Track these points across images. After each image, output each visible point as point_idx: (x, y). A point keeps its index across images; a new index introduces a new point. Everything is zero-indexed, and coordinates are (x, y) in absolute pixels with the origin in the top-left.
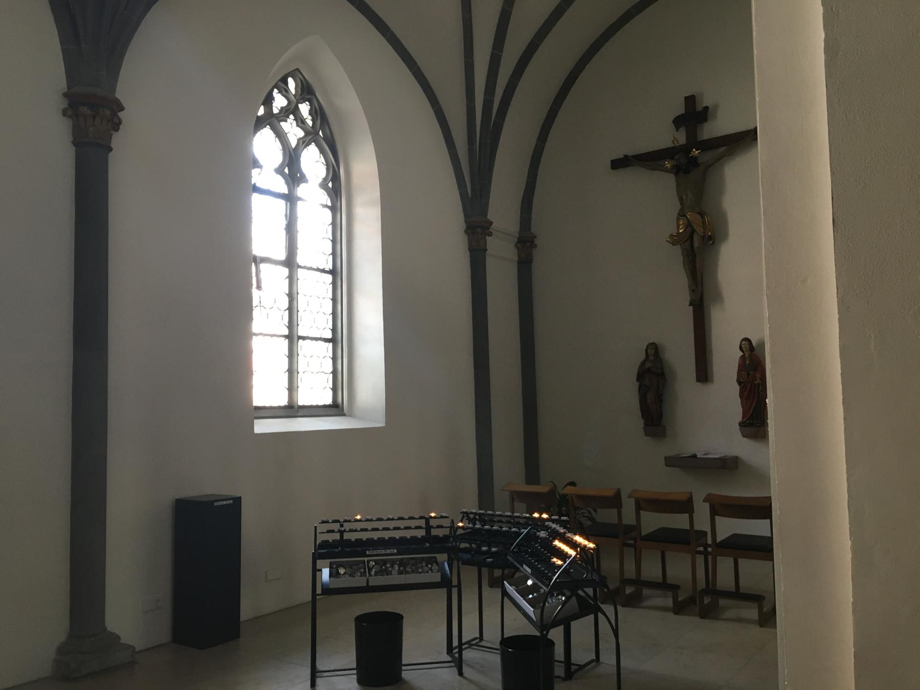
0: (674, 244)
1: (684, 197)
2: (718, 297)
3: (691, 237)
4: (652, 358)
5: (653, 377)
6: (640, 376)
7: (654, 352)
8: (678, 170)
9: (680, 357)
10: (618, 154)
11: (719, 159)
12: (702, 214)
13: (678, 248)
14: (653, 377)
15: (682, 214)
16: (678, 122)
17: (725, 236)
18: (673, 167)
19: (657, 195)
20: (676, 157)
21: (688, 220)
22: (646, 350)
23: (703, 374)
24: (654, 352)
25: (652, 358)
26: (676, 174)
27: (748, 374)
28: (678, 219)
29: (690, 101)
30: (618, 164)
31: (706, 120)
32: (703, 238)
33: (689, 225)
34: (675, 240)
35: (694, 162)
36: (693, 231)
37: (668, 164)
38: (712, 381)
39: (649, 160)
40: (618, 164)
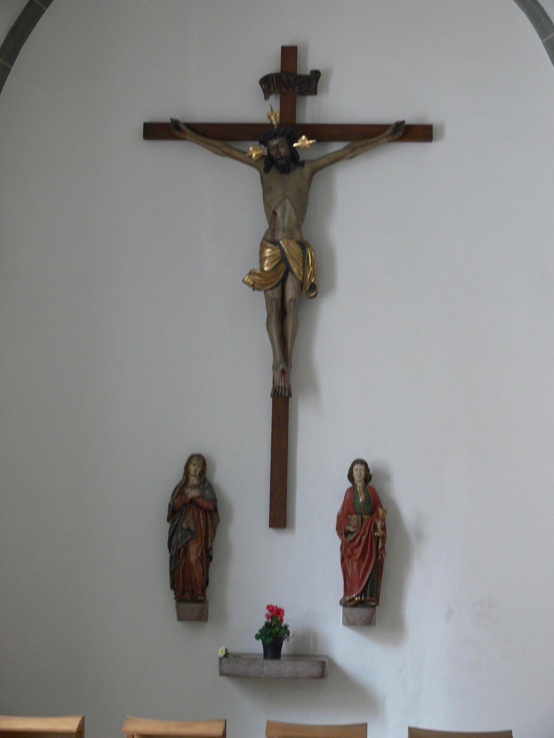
0: (254, 287)
1: (279, 212)
2: (312, 385)
3: (283, 282)
4: (193, 481)
5: (194, 518)
6: (175, 512)
7: (198, 468)
8: (269, 165)
9: (243, 486)
10: (163, 115)
11: (336, 159)
12: (303, 245)
13: (260, 296)
14: (194, 518)
15: (270, 239)
16: (269, 84)
17: (331, 287)
18: (261, 157)
19: (228, 198)
20: (274, 142)
21: (282, 252)
22: (187, 467)
23: (280, 515)
24: (198, 468)
25: (193, 481)
26: (267, 170)
27: (362, 520)
28: (263, 247)
29: (289, 54)
30: (154, 131)
31: (314, 92)
32: (302, 285)
33: (283, 259)
34: (258, 281)
35: (294, 160)
36: (288, 270)
37: (254, 150)
38: (293, 527)
39: (220, 136)
40: (154, 131)
